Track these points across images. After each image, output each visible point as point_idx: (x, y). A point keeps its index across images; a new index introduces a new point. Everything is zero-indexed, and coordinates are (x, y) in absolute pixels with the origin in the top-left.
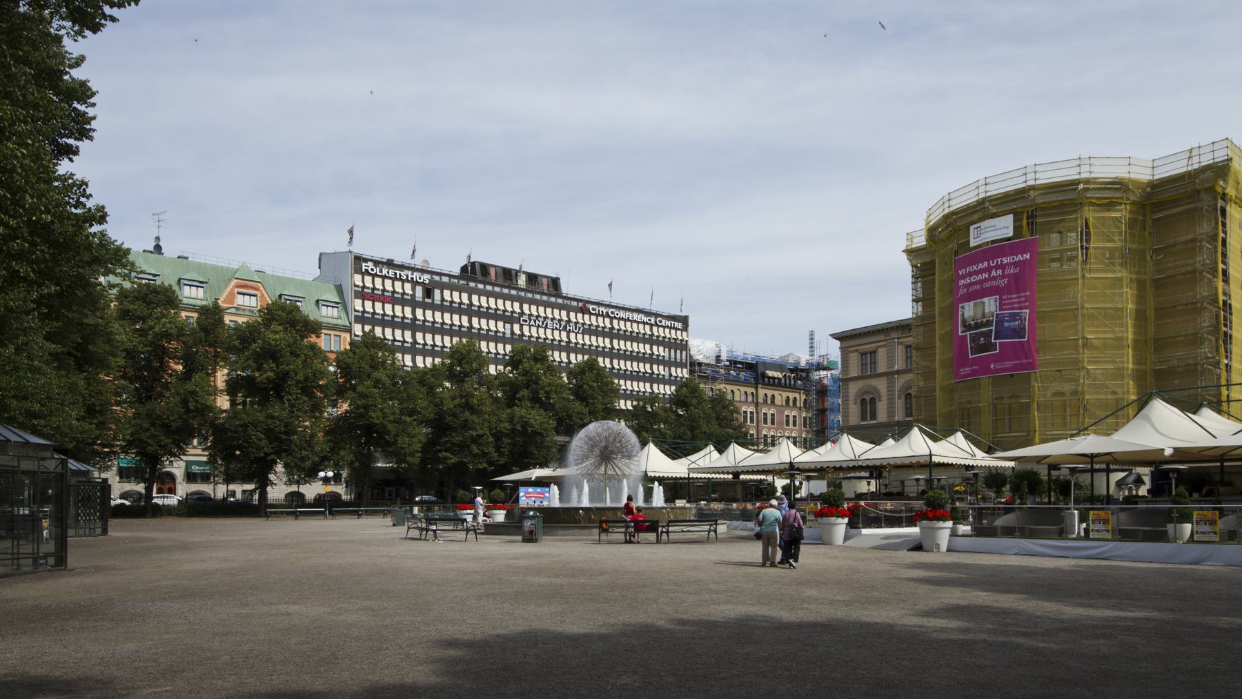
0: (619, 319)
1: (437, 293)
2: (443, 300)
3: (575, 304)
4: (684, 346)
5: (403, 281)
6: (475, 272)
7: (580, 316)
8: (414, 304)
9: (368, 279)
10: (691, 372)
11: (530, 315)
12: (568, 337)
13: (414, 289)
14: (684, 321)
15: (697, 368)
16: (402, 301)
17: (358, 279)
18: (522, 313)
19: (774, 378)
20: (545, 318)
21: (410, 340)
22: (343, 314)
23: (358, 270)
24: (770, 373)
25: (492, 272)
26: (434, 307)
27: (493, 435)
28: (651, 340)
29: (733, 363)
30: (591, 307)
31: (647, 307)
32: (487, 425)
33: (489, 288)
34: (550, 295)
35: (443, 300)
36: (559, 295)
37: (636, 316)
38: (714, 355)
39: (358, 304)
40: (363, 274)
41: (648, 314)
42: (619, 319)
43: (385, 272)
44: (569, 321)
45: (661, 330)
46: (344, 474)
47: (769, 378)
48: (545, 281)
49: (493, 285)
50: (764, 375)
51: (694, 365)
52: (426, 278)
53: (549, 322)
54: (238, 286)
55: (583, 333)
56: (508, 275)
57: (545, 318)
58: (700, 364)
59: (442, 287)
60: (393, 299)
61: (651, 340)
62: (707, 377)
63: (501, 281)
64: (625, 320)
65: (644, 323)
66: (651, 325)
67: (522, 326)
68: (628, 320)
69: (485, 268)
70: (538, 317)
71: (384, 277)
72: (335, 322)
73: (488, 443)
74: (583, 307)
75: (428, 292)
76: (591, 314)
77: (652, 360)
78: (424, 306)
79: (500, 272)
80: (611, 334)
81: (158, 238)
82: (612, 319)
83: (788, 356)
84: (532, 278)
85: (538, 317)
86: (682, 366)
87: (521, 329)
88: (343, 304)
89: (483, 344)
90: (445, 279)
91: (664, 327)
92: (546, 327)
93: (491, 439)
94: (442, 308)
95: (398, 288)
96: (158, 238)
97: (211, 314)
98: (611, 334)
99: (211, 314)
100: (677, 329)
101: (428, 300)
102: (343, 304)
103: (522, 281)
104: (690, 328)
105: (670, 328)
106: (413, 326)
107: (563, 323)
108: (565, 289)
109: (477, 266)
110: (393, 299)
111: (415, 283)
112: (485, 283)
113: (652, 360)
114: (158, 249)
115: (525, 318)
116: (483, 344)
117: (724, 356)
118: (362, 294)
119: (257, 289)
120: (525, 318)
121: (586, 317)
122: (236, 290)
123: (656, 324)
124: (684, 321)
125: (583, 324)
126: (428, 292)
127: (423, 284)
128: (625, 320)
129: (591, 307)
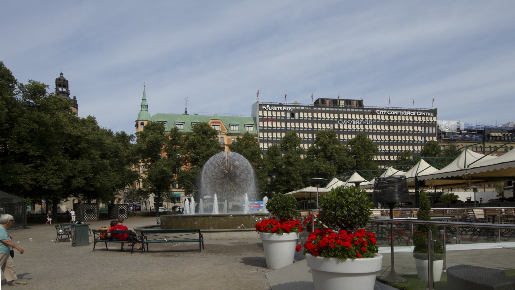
0: (394, 115)
1: (297, 115)
2: (299, 117)
3: (369, 111)
4: (434, 125)
5: (281, 111)
6: (320, 103)
7: (371, 116)
8: (286, 121)
9: (265, 113)
10: (439, 138)
11: (344, 119)
12: (364, 127)
13: (286, 114)
14: (435, 112)
15: (443, 136)
16: (281, 120)
17: (261, 113)
18: (339, 119)
19: (496, 137)
20: (352, 119)
21: (311, 138)
22: (255, 129)
23: (260, 109)
24: (493, 134)
25: (327, 102)
26: (295, 121)
27: (302, 176)
28: (413, 124)
29: (470, 131)
30: (377, 111)
31: (410, 107)
32: (298, 171)
33: (353, 110)
34: (359, 109)
35: (299, 117)
36: (363, 109)
37: (397, 113)
38: (456, 128)
39: (261, 124)
40: (263, 111)
41: (412, 111)
42: (394, 115)
43: (272, 108)
44: (365, 119)
45: (419, 118)
46: (39, 199)
47: (493, 137)
48: (355, 102)
49: (355, 108)
50: (489, 136)
51: (440, 134)
52: (291, 109)
53: (354, 121)
54: (212, 123)
55: (373, 125)
56: (335, 102)
57: (352, 119)
58: (444, 133)
59: (299, 111)
60: (276, 120)
61: (413, 124)
62: (449, 140)
63: (332, 105)
64: (397, 115)
65: (409, 116)
66: (413, 116)
67: (339, 125)
68: (399, 115)
69: (323, 101)
70: (348, 119)
71: (272, 111)
72: (238, 132)
73: (299, 180)
74: (373, 112)
75: (293, 115)
76: (377, 114)
77: (413, 134)
78: (291, 121)
79: (331, 101)
80: (389, 123)
81: (186, 108)
82: (389, 116)
83: (508, 124)
84: (348, 102)
85: (348, 119)
86: (433, 135)
87: (339, 126)
88: (256, 125)
89: (371, 137)
90: (302, 108)
91: (421, 116)
92: (352, 124)
93: (300, 178)
94: (299, 121)
95: (279, 115)
96: (186, 108)
97: (175, 131)
98: (389, 123)
99: (175, 131)
100: (429, 116)
101: (292, 118)
102: (256, 125)
103: (342, 103)
104: (438, 115)
105: (425, 116)
106: (389, 133)
107: (361, 121)
108: (366, 104)
109: (320, 101)
110: (276, 120)
111: (286, 112)
112: (351, 108)
113: (413, 134)
114: (186, 112)
115: (341, 120)
116: (341, 137)
117: (462, 128)
118: (263, 120)
119: (220, 123)
120: (341, 120)
121: (375, 116)
122: (212, 124)
123: (416, 115)
124: (435, 112)
125: (373, 120)
126: (293, 115)
127: (290, 111)
128: (397, 115)
129: (377, 111)
